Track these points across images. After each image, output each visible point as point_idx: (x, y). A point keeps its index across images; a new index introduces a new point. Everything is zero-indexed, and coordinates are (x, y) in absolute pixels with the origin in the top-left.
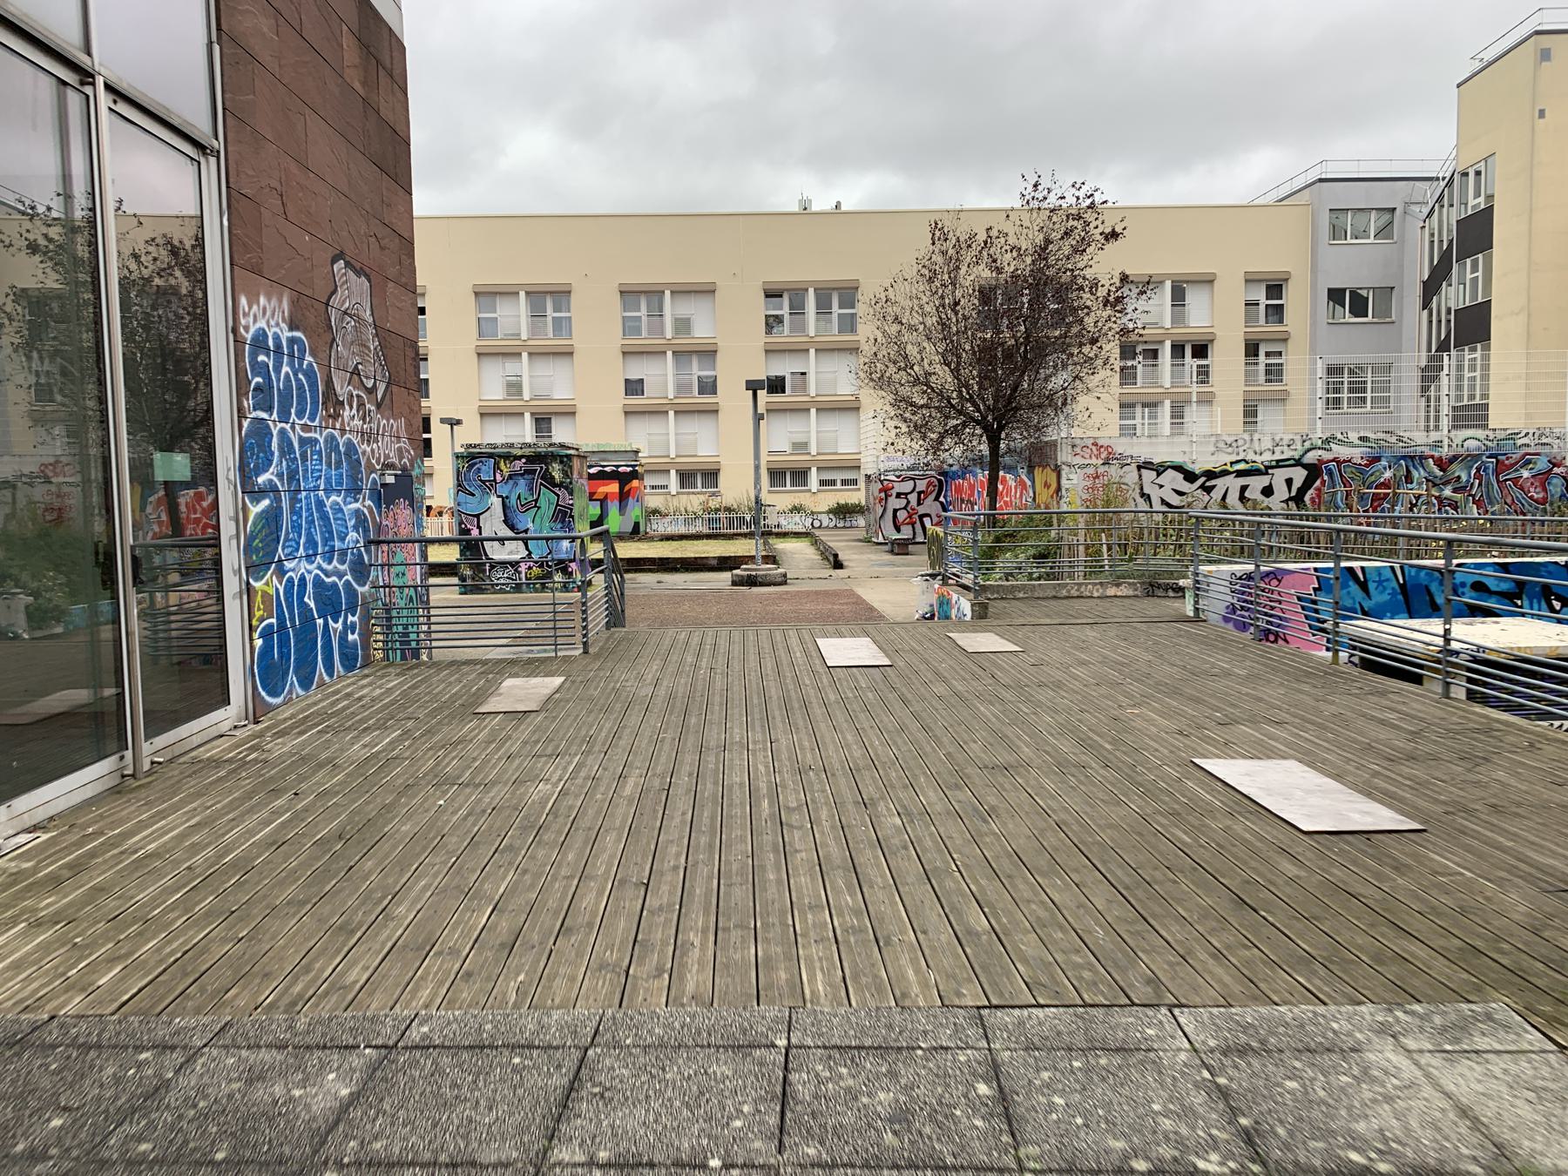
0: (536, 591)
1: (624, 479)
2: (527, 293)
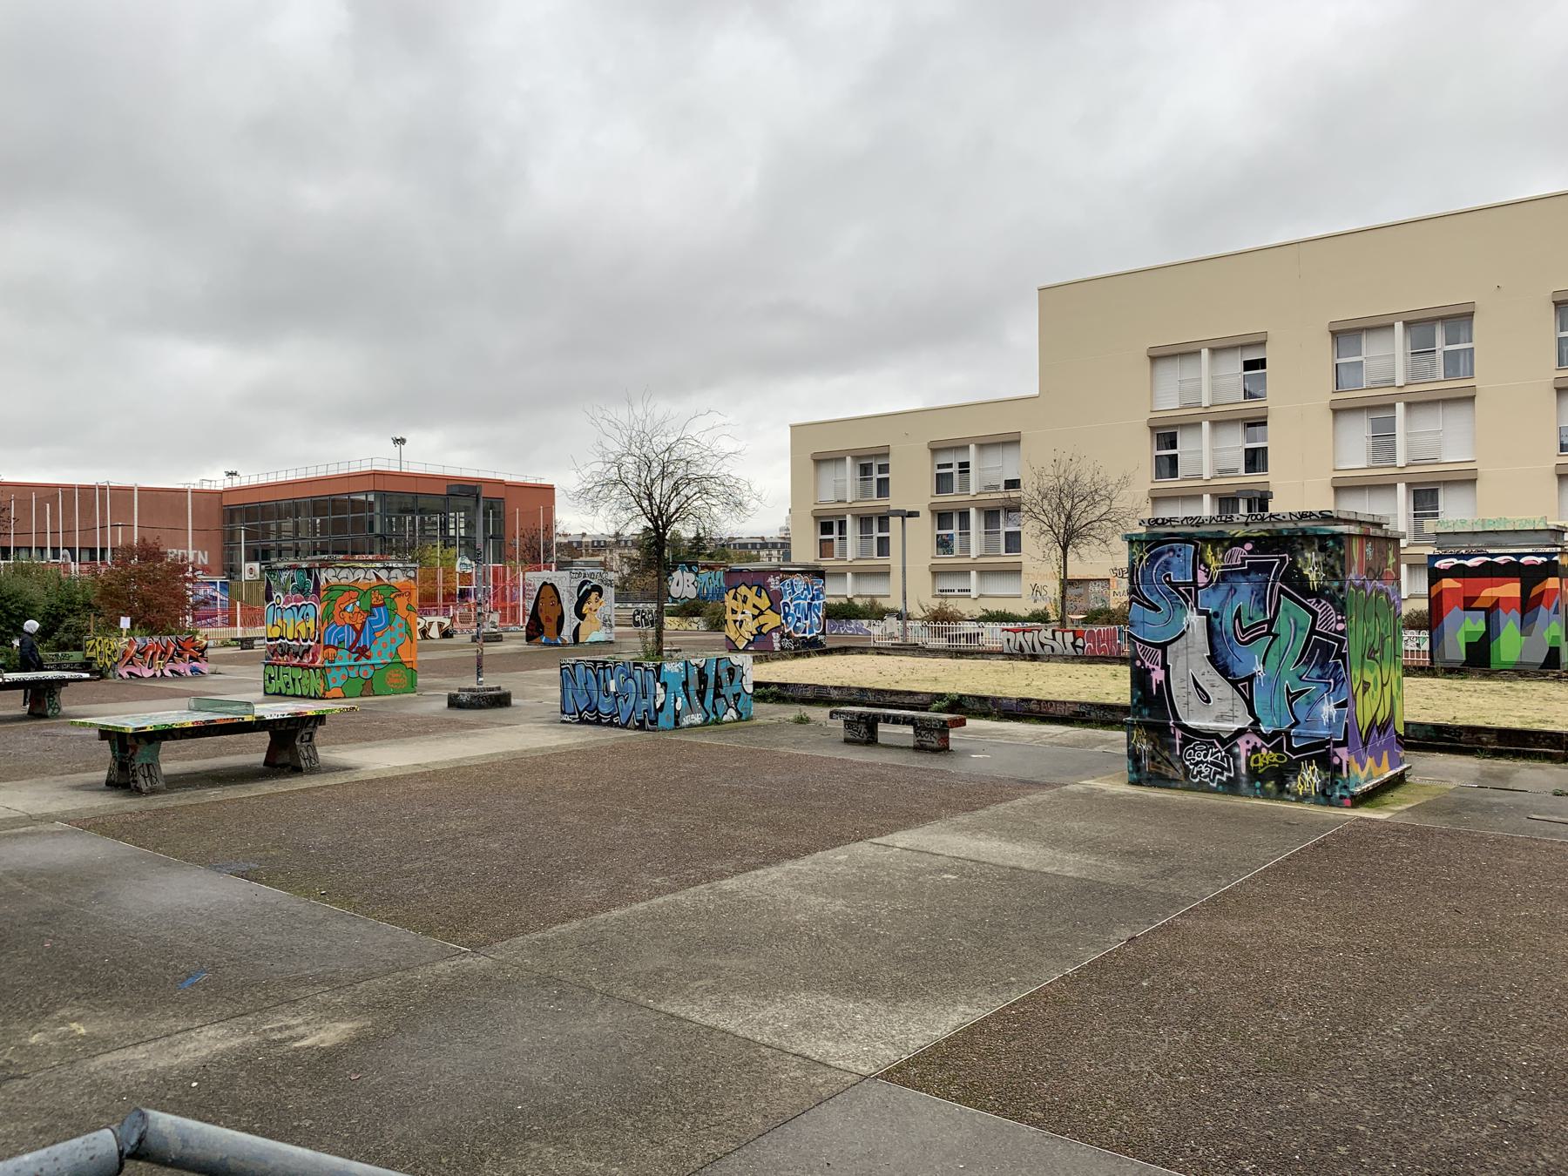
0: (1266, 795)
1: (1530, 576)
2: (1407, 324)
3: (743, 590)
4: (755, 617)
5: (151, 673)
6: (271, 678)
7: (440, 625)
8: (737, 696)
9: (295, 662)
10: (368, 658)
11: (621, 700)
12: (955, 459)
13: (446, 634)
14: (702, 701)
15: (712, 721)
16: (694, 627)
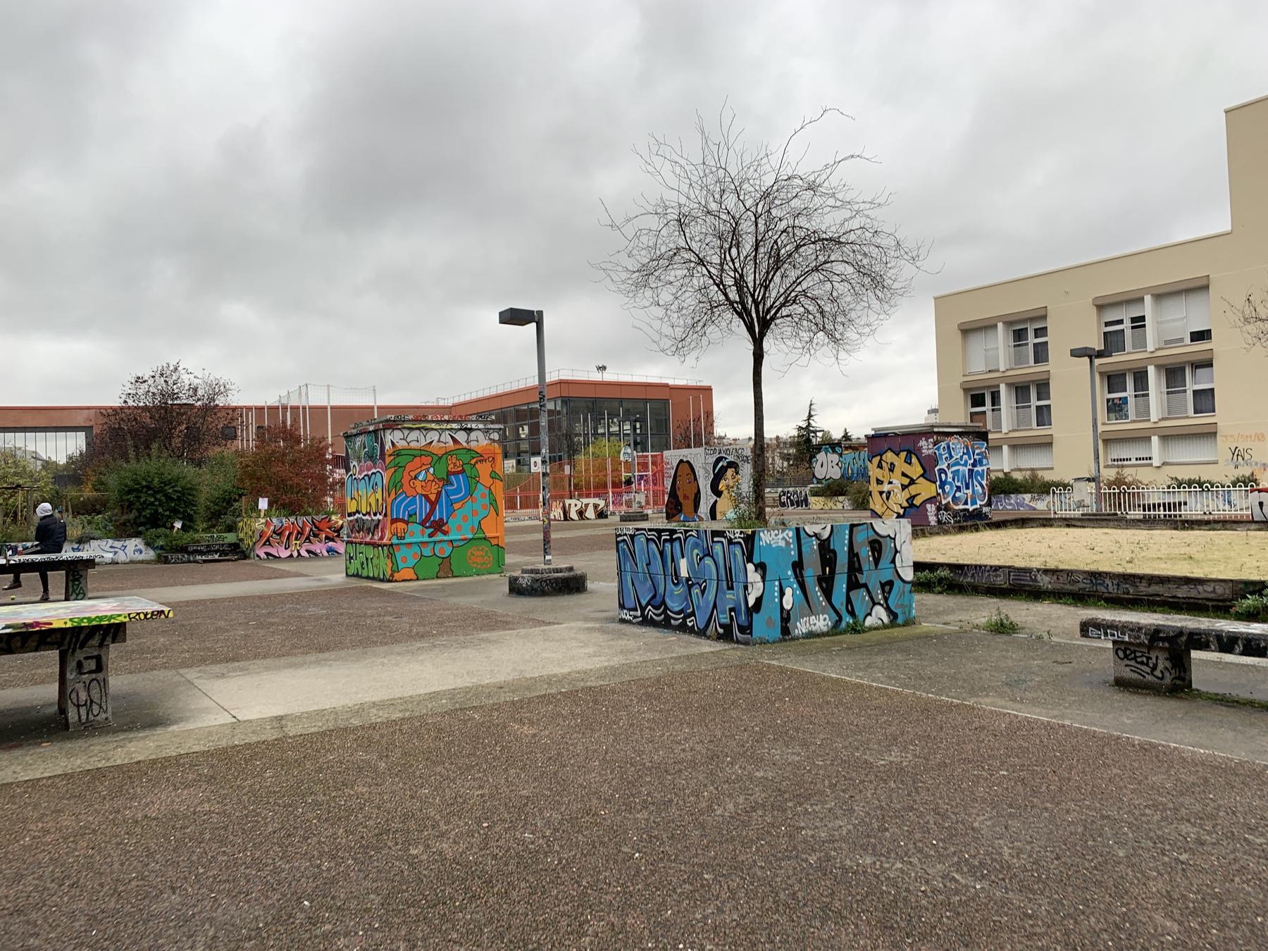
3: (889, 457)
4: (904, 487)
5: (288, 553)
6: (351, 558)
7: (596, 506)
8: (887, 586)
9: (368, 539)
10: (445, 533)
11: (696, 591)
12: (1126, 314)
13: (601, 515)
14: (828, 593)
15: (847, 626)
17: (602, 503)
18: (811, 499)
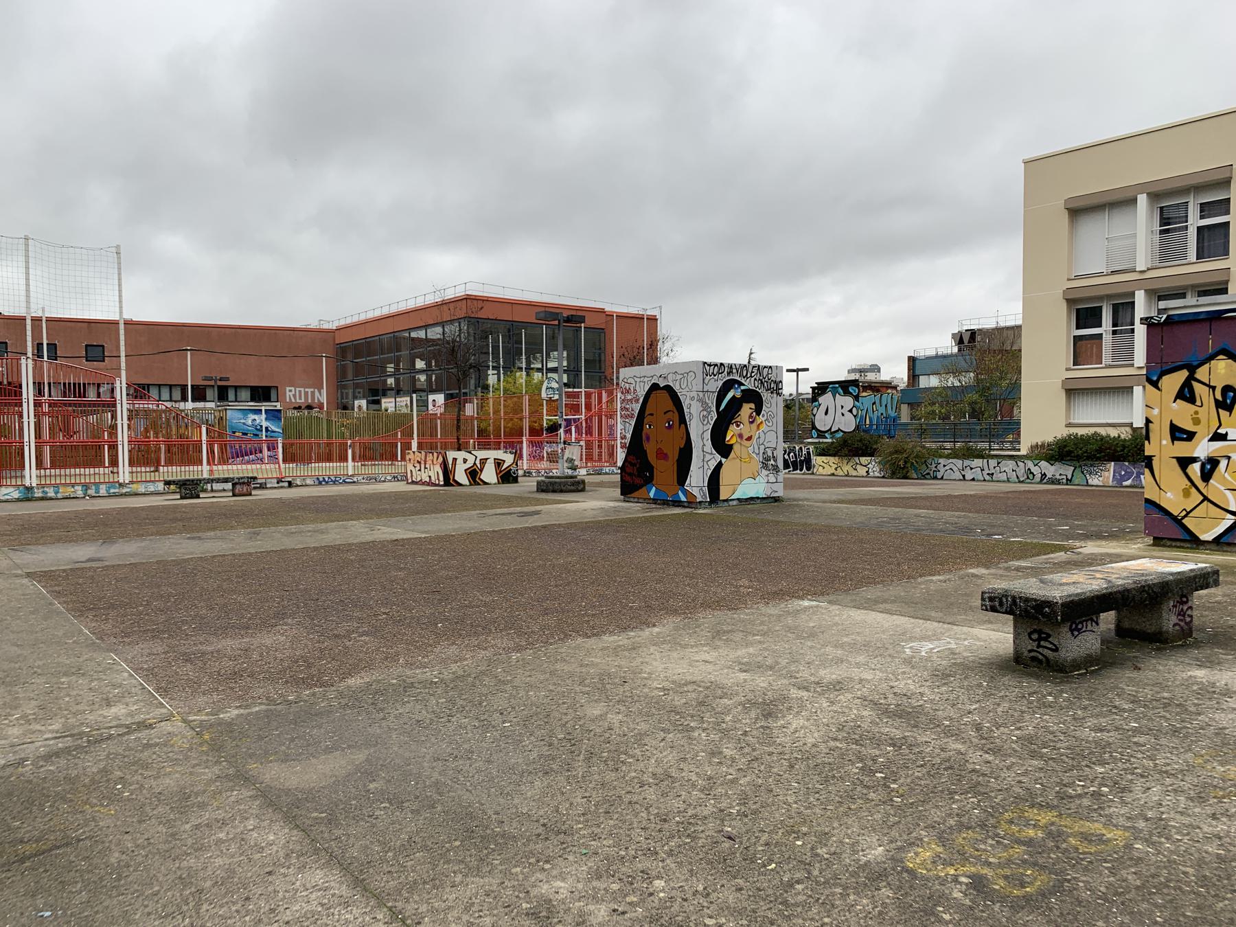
7: (498, 463)
13: (507, 477)
16: (862, 471)
17: (509, 459)
18: (817, 460)
